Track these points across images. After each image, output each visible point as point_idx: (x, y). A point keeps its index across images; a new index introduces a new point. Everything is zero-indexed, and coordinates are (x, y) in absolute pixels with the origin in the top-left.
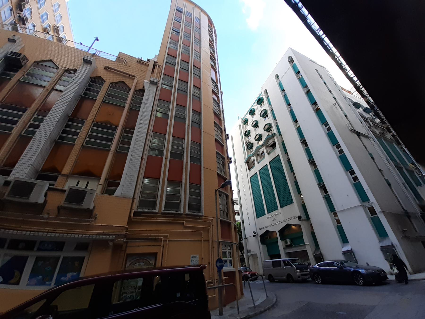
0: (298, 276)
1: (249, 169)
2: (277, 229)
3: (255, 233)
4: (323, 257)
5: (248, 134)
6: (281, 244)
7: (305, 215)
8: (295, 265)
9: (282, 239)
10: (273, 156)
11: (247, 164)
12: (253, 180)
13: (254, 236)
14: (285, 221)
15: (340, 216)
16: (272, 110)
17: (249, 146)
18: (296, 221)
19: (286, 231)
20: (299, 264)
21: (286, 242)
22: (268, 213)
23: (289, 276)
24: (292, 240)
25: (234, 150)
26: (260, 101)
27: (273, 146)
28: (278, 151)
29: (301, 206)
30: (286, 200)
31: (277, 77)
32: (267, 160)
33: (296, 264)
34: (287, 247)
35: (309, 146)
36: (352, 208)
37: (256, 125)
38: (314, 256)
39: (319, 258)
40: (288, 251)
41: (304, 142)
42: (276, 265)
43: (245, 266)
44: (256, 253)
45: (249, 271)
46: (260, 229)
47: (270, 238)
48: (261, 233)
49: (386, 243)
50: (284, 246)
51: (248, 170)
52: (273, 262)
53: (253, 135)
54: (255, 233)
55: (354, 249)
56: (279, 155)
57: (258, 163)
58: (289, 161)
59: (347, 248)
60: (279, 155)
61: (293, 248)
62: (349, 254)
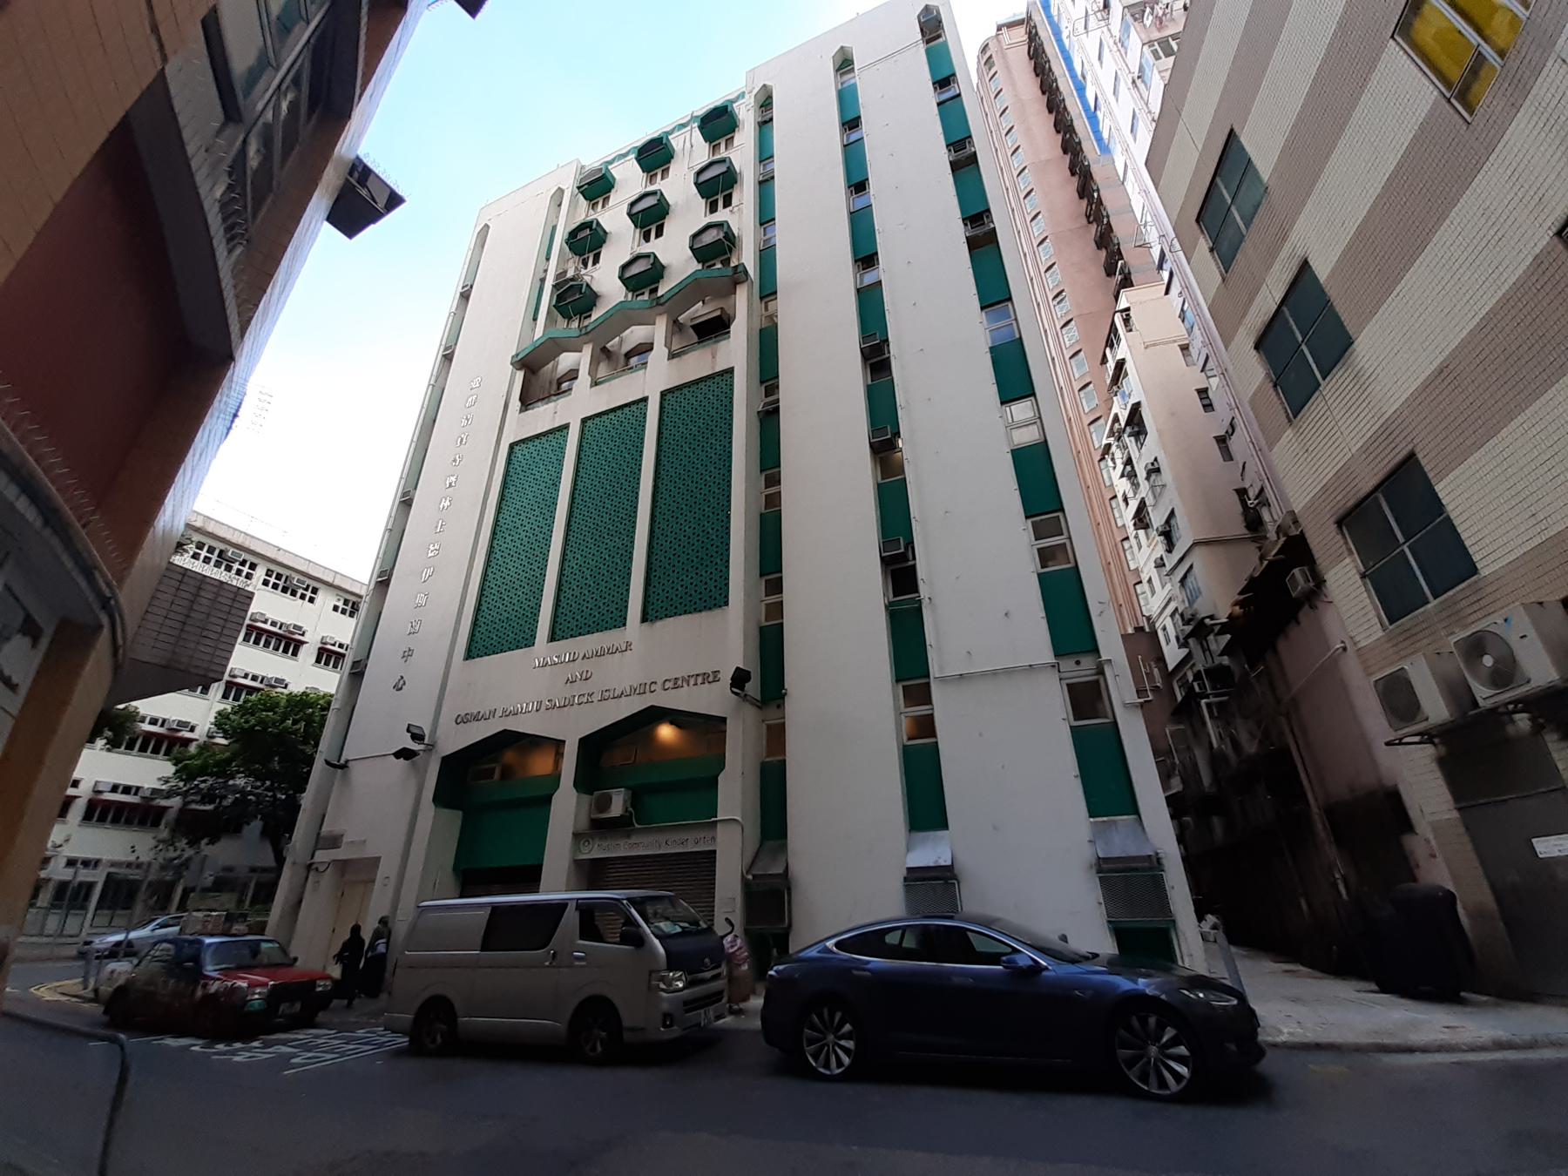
0: (666, 1016)
1: (527, 402)
2: (573, 728)
3: (418, 737)
4: (789, 889)
5: (587, 241)
6: (566, 808)
7: (765, 679)
8: (663, 937)
9: (582, 784)
10: (698, 364)
11: (520, 375)
12: (525, 463)
13: (404, 754)
14: (643, 689)
15: (943, 703)
16: (765, 184)
17: (573, 299)
18: (711, 700)
19: (611, 752)
20: (684, 933)
21: (604, 804)
22: (553, 638)
23: (595, 1012)
24: (635, 799)
25: (465, 296)
26: (717, 124)
27: (714, 329)
28: (735, 352)
29: (755, 633)
30: (686, 584)
31: (844, 64)
32: (656, 377)
33: (665, 926)
34: (600, 827)
35: (785, 488)
36: (1008, 671)
37: (650, 217)
38: (746, 884)
39: (770, 899)
40: (596, 850)
41: (876, 359)
42: (505, 930)
43: (260, 928)
44: (370, 852)
45: (271, 967)
46: (462, 720)
47: (504, 776)
48: (454, 740)
49: (1122, 843)
50: (584, 824)
51: (515, 403)
52: (495, 908)
53: (615, 255)
54: (418, 737)
55: (966, 866)
56: (730, 371)
57: (595, 383)
58: (769, 419)
59: (932, 852)
60: (730, 371)
61: (634, 840)
62: (932, 884)
